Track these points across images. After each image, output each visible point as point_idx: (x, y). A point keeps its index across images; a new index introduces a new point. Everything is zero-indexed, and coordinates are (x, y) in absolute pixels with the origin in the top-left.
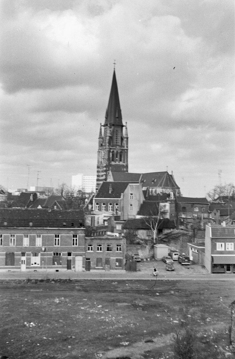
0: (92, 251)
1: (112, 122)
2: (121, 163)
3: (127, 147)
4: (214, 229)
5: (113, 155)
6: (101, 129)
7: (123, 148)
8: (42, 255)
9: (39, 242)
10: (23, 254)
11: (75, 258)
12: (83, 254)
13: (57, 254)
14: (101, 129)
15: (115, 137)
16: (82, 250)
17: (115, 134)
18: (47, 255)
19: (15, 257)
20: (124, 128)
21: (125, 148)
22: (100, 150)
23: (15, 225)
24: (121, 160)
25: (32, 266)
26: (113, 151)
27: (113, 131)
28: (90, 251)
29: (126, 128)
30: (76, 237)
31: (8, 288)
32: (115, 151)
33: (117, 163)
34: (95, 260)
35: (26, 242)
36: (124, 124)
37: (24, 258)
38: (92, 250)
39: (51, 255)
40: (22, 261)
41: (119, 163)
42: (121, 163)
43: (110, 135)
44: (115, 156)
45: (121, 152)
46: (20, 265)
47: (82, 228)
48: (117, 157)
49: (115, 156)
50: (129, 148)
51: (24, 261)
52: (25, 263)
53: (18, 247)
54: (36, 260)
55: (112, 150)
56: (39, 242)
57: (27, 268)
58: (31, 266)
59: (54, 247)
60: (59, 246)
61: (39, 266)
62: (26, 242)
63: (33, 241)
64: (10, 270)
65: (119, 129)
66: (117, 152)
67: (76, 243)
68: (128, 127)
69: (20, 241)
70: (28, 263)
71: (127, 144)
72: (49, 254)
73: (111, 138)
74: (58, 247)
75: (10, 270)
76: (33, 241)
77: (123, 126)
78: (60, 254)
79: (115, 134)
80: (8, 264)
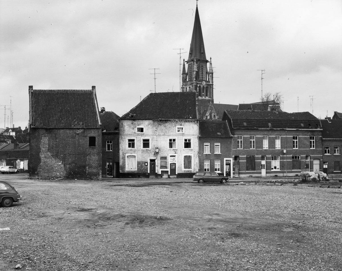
0: (329, 154)
1: (198, 57)
2: (207, 98)
3: (212, 82)
4: (247, 167)
5: (200, 90)
6: (184, 65)
7: (209, 84)
8: (281, 158)
9: (278, 144)
10: (263, 158)
11: (313, 161)
12: (320, 157)
13: (296, 157)
14: (184, 65)
15: (201, 73)
16: (319, 153)
17: (201, 69)
18: (287, 158)
19: (246, 161)
20: (208, 64)
21: (211, 83)
22: (184, 86)
23: (255, 126)
24: (207, 95)
25: (272, 170)
26: (200, 86)
27: (199, 66)
28: (327, 154)
29: (211, 64)
30: (313, 139)
31: (109, 219)
32: (202, 86)
33: (204, 98)
34: (339, 160)
35: (266, 144)
36: (208, 58)
37: (263, 162)
38: (328, 153)
39: (289, 158)
40: (262, 165)
41: (205, 98)
42: (207, 98)
43: (197, 70)
44: (202, 91)
45: (207, 87)
46: (261, 170)
47: (319, 129)
48: (203, 92)
49: (202, 91)
50: (214, 83)
51: (264, 165)
52: (265, 167)
53: (258, 150)
54: (276, 164)
55: (198, 85)
56: (278, 144)
57: (267, 173)
58: (271, 171)
59: (294, 150)
60: (297, 148)
61: (279, 170)
62: (266, 144)
63: (272, 143)
64: (251, 175)
65: (204, 64)
66: (203, 87)
67: (313, 146)
68: (212, 62)
69: (260, 143)
70: (268, 167)
71: (212, 79)
72: (289, 157)
73: (197, 73)
74: (297, 150)
75: (251, 175)
76: (272, 143)
77: (207, 61)
78: (299, 157)
79: (201, 69)
80: (249, 169)
